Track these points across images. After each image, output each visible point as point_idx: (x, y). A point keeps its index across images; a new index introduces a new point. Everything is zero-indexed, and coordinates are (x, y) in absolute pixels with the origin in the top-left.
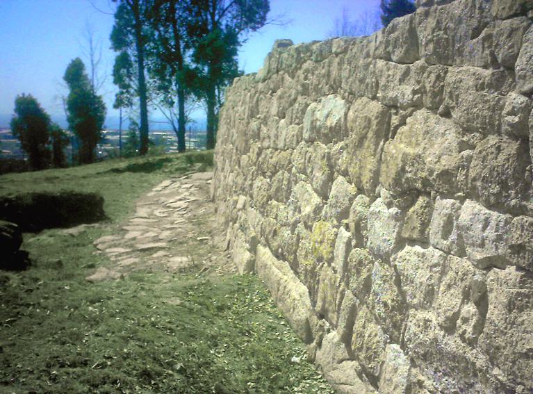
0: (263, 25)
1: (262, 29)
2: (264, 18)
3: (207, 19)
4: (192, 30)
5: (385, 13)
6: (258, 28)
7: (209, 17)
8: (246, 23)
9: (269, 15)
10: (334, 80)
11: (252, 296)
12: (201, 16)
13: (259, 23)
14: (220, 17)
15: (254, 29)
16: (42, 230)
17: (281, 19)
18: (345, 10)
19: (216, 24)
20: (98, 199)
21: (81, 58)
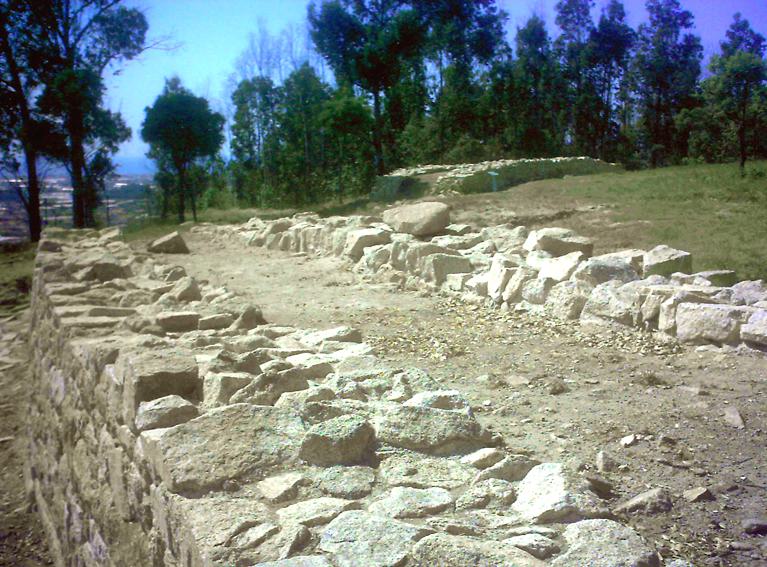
0: (140, 50)
1: (142, 55)
2: (141, 40)
3: (57, 42)
4: (35, 58)
5: (315, 28)
6: (135, 54)
7: (60, 40)
8: (117, 49)
9: (149, 35)
10: (121, 342)
11: (24, 539)
12: (49, 40)
13: (134, 47)
14: (77, 40)
15: (129, 56)
16: (83, 158)
17: (167, 42)
18: (260, 21)
19: (71, 50)
20: (539, 22)
21: (554, 20)
